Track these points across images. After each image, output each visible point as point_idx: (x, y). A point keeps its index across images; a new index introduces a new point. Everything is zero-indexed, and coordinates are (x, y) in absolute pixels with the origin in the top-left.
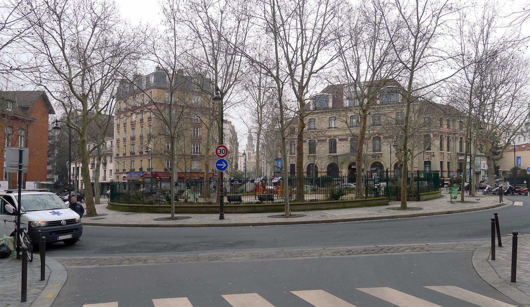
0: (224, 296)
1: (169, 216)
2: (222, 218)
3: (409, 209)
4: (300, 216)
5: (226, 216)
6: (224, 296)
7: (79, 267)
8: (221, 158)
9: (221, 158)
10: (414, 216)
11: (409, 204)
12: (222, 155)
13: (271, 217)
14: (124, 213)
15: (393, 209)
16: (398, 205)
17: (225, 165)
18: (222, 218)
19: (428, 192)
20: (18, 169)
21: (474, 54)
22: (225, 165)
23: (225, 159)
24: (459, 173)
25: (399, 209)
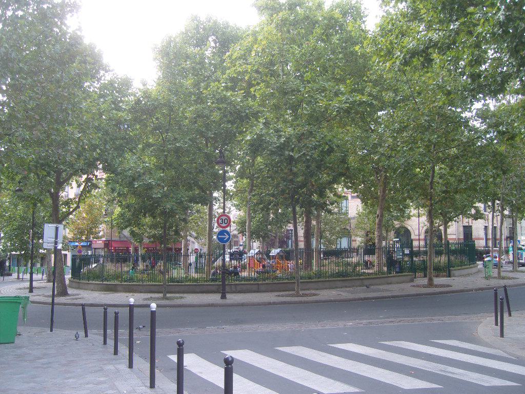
0: (169, 356)
1: (161, 295)
2: (224, 297)
3: (436, 286)
4: (314, 295)
5: (228, 296)
6: (169, 356)
7: (392, 324)
8: (223, 229)
9: (223, 229)
10: (441, 293)
11: (437, 281)
12: (224, 225)
13: (279, 296)
14: (103, 292)
15: (418, 286)
16: (425, 281)
17: (227, 237)
18: (224, 297)
19: (461, 266)
20: (53, 244)
21: (155, 83)
22: (227, 237)
23: (228, 229)
24: (508, 241)
25: (424, 286)
